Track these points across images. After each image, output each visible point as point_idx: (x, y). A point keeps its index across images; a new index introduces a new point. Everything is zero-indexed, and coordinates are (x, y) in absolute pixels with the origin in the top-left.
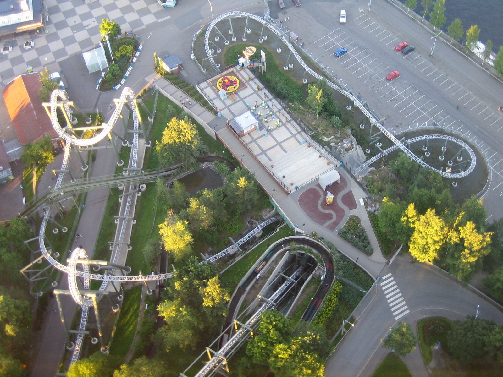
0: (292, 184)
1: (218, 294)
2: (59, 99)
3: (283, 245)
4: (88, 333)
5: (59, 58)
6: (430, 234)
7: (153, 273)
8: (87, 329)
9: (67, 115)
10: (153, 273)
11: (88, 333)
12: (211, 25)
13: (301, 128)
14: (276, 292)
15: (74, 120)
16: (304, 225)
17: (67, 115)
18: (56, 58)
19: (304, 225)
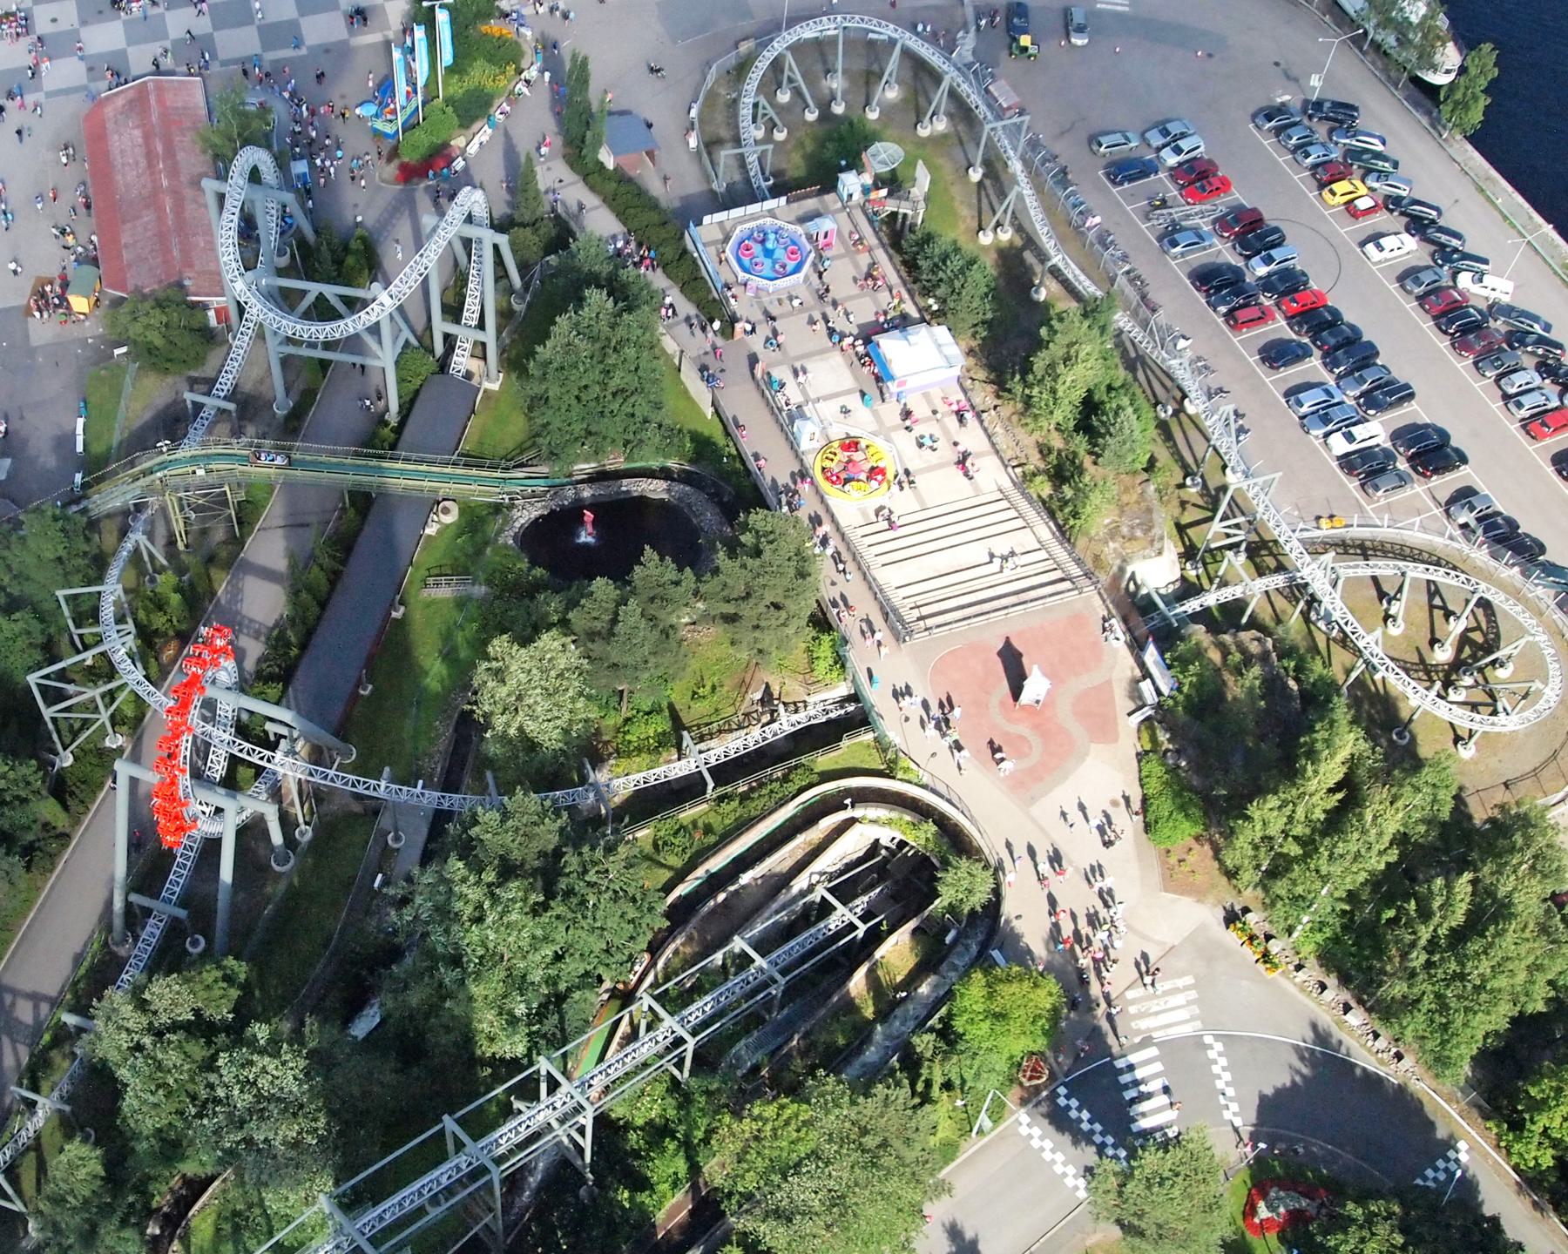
0: (343, 97)
1: (952, 909)
2: (254, 176)
3: (848, 801)
4: (182, 913)
5: (274, 48)
6: (847, 1125)
7: (420, 782)
8: (183, 902)
9: (269, 229)
10: (420, 782)
11: (182, 913)
12: (775, 44)
13: (880, 239)
14: (792, 943)
15: (281, 253)
16: (934, 755)
17: (269, 229)
18: (267, 44)
19: (934, 755)
